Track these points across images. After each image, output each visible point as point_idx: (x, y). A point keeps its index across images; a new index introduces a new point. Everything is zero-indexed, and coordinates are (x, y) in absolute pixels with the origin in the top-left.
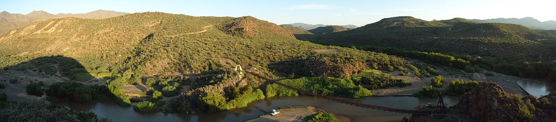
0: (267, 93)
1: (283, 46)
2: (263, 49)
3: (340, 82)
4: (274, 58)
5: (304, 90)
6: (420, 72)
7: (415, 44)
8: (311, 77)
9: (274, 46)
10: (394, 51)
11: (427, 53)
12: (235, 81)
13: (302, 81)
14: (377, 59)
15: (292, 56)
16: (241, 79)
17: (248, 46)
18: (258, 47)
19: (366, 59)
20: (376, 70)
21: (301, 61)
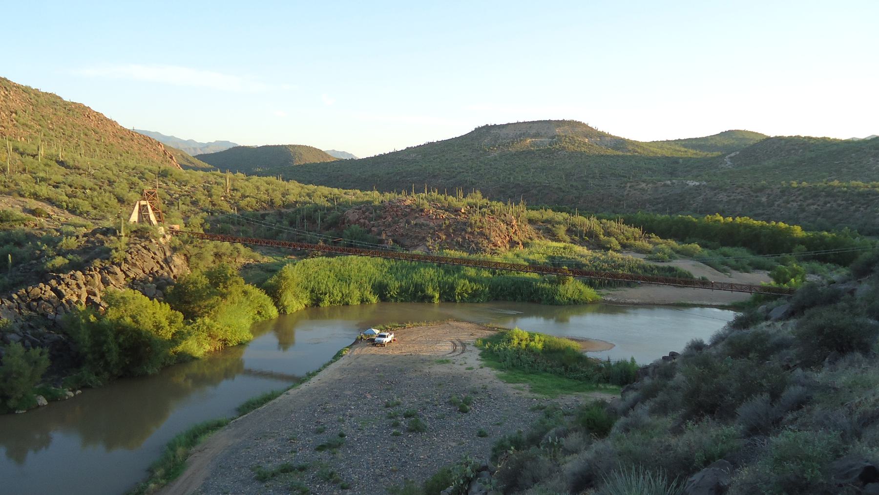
7: (620, 201)
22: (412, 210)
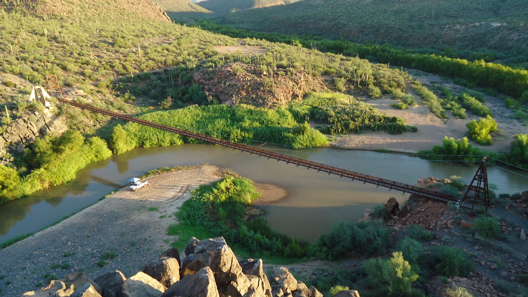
0: (116, 145)
1: (143, 38)
2: (96, 47)
3: (265, 115)
4: (123, 66)
5: (195, 131)
6: (442, 104)
8: (206, 105)
9: (122, 40)
10: (386, 54)
11: (465, 62)
12: (35, 126)
13: (189, 114)
14: (347, 71)
15: (165, 62)
16: (50, 119)
17: (55, 38)
18: (83, 42)
19: (323, 68)
20: (343, 95)
21: (184, 72)
22: (230, 74)
